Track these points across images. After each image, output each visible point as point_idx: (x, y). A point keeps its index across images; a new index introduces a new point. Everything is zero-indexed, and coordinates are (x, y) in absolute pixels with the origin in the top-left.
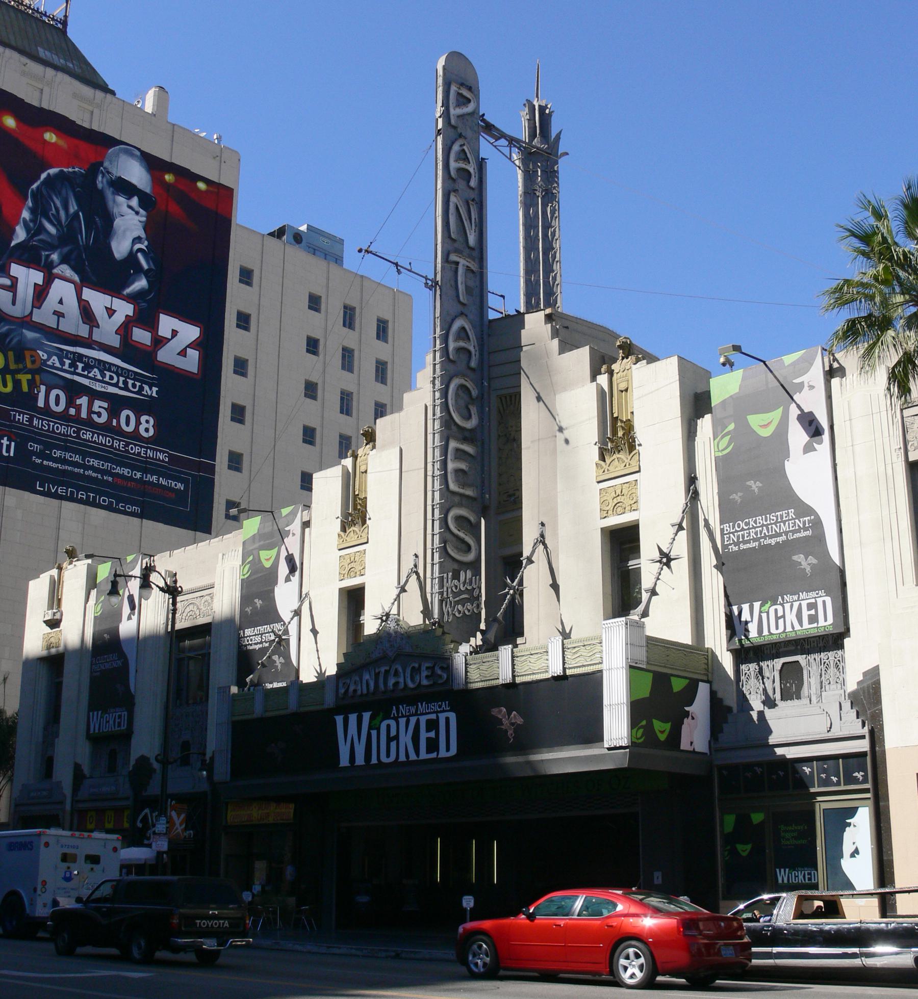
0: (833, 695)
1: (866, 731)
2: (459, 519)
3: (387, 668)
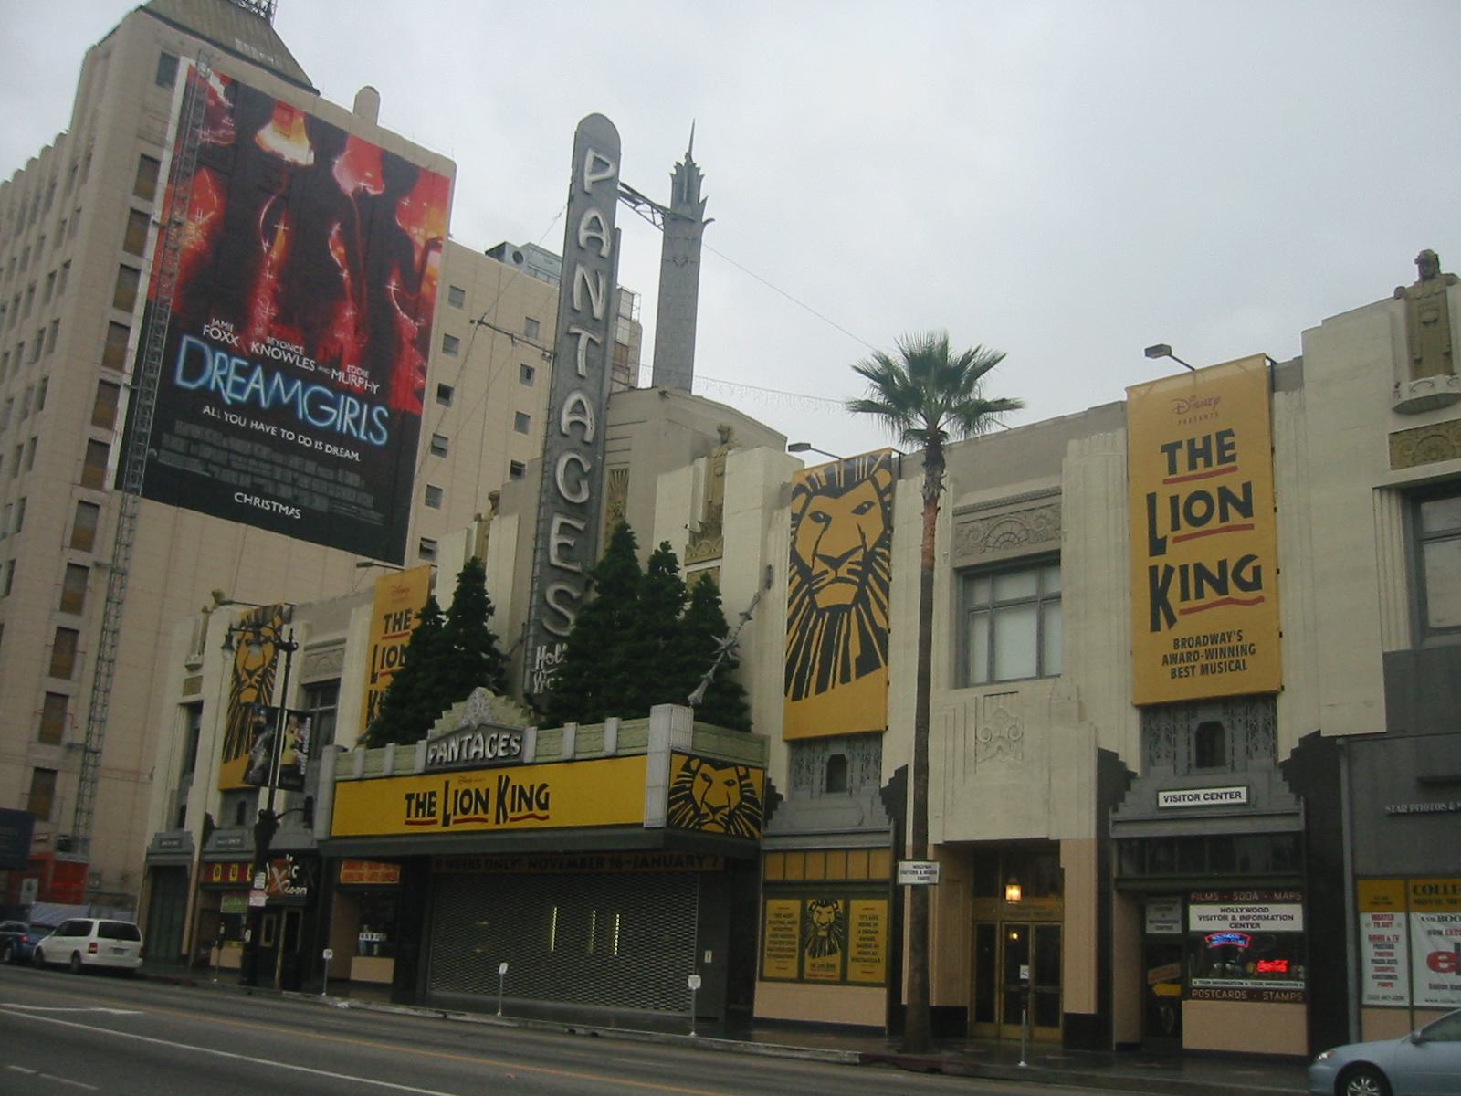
0: (870, 788)
3: (470, 737)
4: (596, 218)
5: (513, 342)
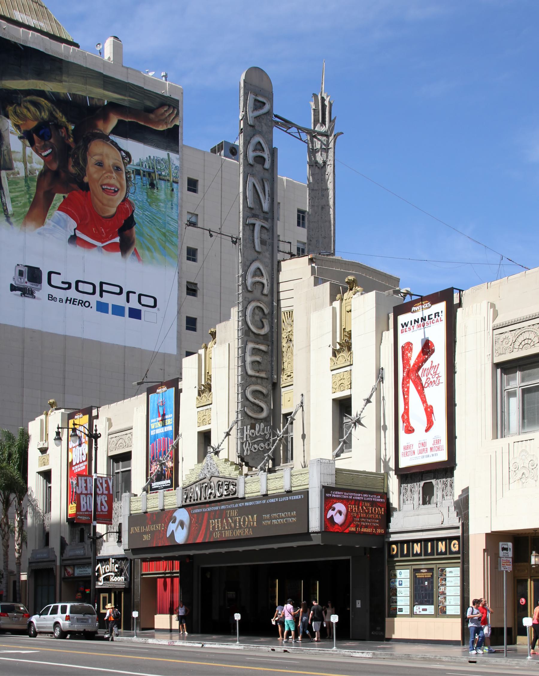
1: (460, 524)
2: (255, 393)
4: (259, 143)
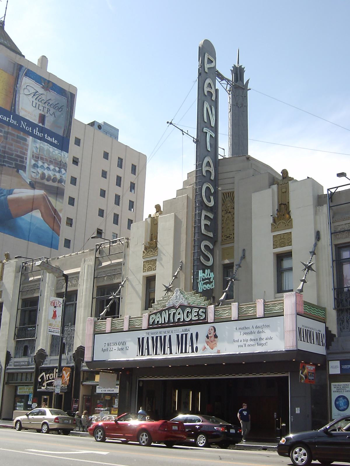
2: (206, 247)
5: (183, 134)
